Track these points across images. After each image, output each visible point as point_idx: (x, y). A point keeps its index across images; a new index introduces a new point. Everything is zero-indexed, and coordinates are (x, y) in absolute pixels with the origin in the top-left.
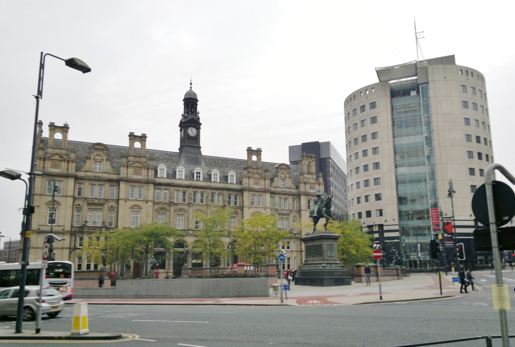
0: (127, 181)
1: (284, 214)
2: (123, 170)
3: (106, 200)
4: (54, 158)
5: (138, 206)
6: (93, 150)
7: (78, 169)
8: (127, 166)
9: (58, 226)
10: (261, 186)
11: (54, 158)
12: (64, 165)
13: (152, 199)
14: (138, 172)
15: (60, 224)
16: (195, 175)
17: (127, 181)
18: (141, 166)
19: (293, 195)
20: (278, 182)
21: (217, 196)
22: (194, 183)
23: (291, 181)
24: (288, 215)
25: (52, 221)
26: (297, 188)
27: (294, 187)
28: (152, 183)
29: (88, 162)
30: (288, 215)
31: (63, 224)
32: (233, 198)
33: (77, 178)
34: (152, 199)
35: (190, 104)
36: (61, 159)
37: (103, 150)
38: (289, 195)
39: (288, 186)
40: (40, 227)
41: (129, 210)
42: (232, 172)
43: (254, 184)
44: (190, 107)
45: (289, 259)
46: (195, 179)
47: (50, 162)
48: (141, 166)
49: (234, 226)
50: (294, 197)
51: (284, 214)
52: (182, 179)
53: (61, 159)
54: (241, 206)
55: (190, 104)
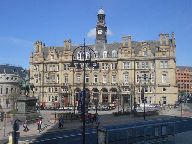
0: (159, 59)
2: (157, 54)
3: (150, 70)
4: (35, 56)
5: (165, 71)
7: (136, 56)
8: (159, 52)
11: (35, 56)
13: (134, 68)
17: (159, 59)
18: (128, 52)
19: (151, 60)
20: (142, 54)
22: (111, 59)
23: (150, 52)
26: (155, 55)
27: (153, 55)
28: (171, 59)
29: (140, 51)
32: (105, 65)
33: (44, 64)
34: (172, 67)
37: (147, 45)
38: (148, 60)
41: (76, 75)
42: (114, 51)
45: (150, 97)
46: (113, 57)
52: (106, 58)
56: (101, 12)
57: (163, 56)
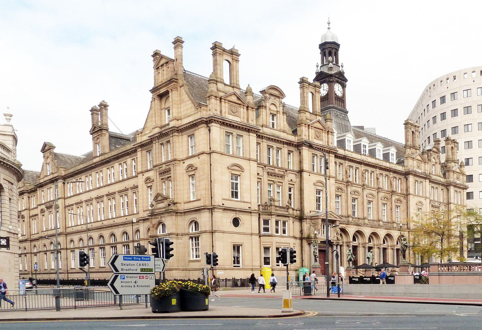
1: (276, 175)
4: (230, 98)
6: (267, 95)
9: (244, 202)
10: (242, 120)
12: (242, 111)
14: (234, 111)
15: (245, 200)
16: (362, 148)
21: (275, 151)
24: (282, 177)
25: (235, 194)
26: (295, 132)
30: (282, 177)
31: (249, 201)
35: (327, 52)
36: (239, 102)
39: (282, 128)
40: (224, 202)
43: (315, 138)
44: (327, 54)
48: (321, 127)
49: (399, 217)
50: (291, 148)
51: (276, 175)
53: (239, 102)
54: (405, 192)
55: (327, 52)
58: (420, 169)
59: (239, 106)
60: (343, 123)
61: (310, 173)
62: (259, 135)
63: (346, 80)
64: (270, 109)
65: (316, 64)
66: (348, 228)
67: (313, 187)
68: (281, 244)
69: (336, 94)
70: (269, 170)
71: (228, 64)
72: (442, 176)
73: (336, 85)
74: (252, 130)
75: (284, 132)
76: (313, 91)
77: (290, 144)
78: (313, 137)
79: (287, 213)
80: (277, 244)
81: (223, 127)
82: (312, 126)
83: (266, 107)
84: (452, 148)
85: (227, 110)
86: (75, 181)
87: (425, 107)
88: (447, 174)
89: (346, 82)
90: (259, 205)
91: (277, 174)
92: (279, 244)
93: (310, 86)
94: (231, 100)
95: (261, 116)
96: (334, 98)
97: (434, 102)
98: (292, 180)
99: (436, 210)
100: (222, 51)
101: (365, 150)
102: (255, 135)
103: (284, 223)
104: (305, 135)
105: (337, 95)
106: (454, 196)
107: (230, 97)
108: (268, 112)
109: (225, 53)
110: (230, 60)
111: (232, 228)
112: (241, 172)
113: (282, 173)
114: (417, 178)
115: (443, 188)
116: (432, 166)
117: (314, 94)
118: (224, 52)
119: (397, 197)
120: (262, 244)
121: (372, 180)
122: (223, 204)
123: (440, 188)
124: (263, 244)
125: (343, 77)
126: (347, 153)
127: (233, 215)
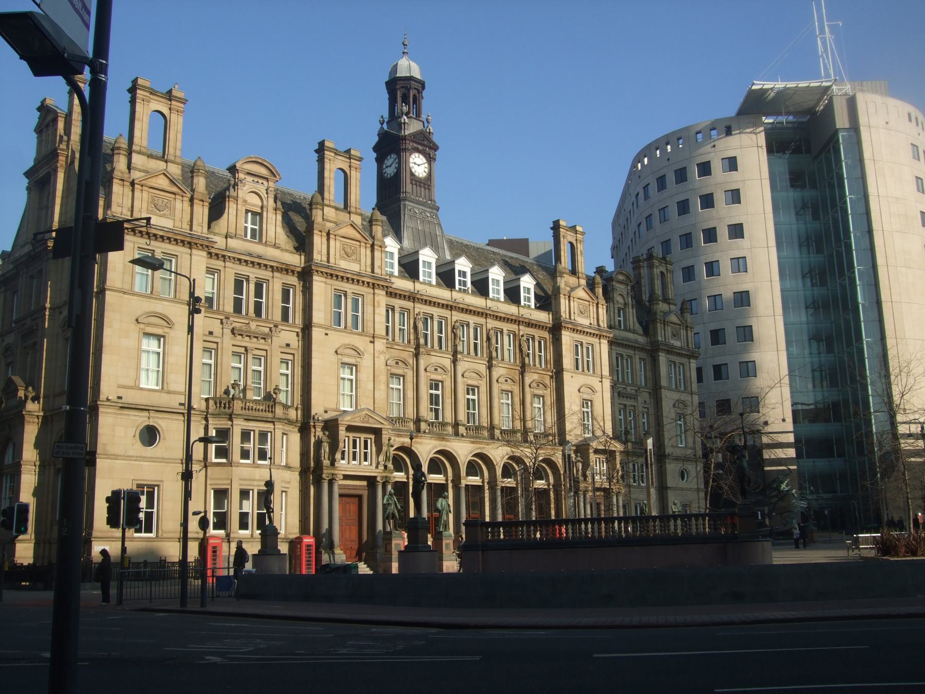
4: (153, 182)
16: (457, 278)
36: (175, 189)
43: (342, 258)
47: (145, 195)
53: (175, 189)
56: (408, 67)
57: (343, 264)
58: (679, 339)
59: (173, 196)
60: (427, 230)
61: (326, 329)
62: (391, 293)
63: (435, 148)
64: (245, 201)
65: (379, 118)
66: (418, 446)
67: (334, 358)
68: (251, 483)
69: (412, 174)
70: (235, 325)
71: (163, 121)
72: (641, 331)
73: (413, 156)
74: (196, 244)
75: (275, 246)
76: (345, 167)
77: (287, 270)
78: (338, 256)
79: (270, 415)
80: (243, 482)
81: (329, 281)
82: (336, 233)
83: (236, 199)
84: (662, 273)
85: (145, 205)
86: (194, 506)
87: (634, 199)
88: (651, 326)
89: (436, 150)
90: (207, 400)
91: (254, 333)
92: (247, 482)
93: (339, 157)
94: (155, 185)
95: (225, 215)
96: (408, 181)
97: (646, 188)
98: (288, 345)
99: (629, 402)
100: (148, 94)
101: (529, 298)
102: (205, 254)
103: (263, 436)
104: (320, 253)
105: (417, 174)
106: (669, 373)
107: (154, 180)
108: (242, 209)
109: (155, 97)
110: (166, 111)
111: (138, 448)
112: (167, 330)
113: (267, 330)
114: (674, 358)
115: (643, 355)
116: (616, 311)
117: (348, 172)
118: (151, 96)
119: (536, 377)
120: (209, 482)
121: (472, 341)
122: (120, 398)
123: (637, 357)
124: (213, 482)
125: (430, 141)
126: (525, 313)
127: (142, 420)
